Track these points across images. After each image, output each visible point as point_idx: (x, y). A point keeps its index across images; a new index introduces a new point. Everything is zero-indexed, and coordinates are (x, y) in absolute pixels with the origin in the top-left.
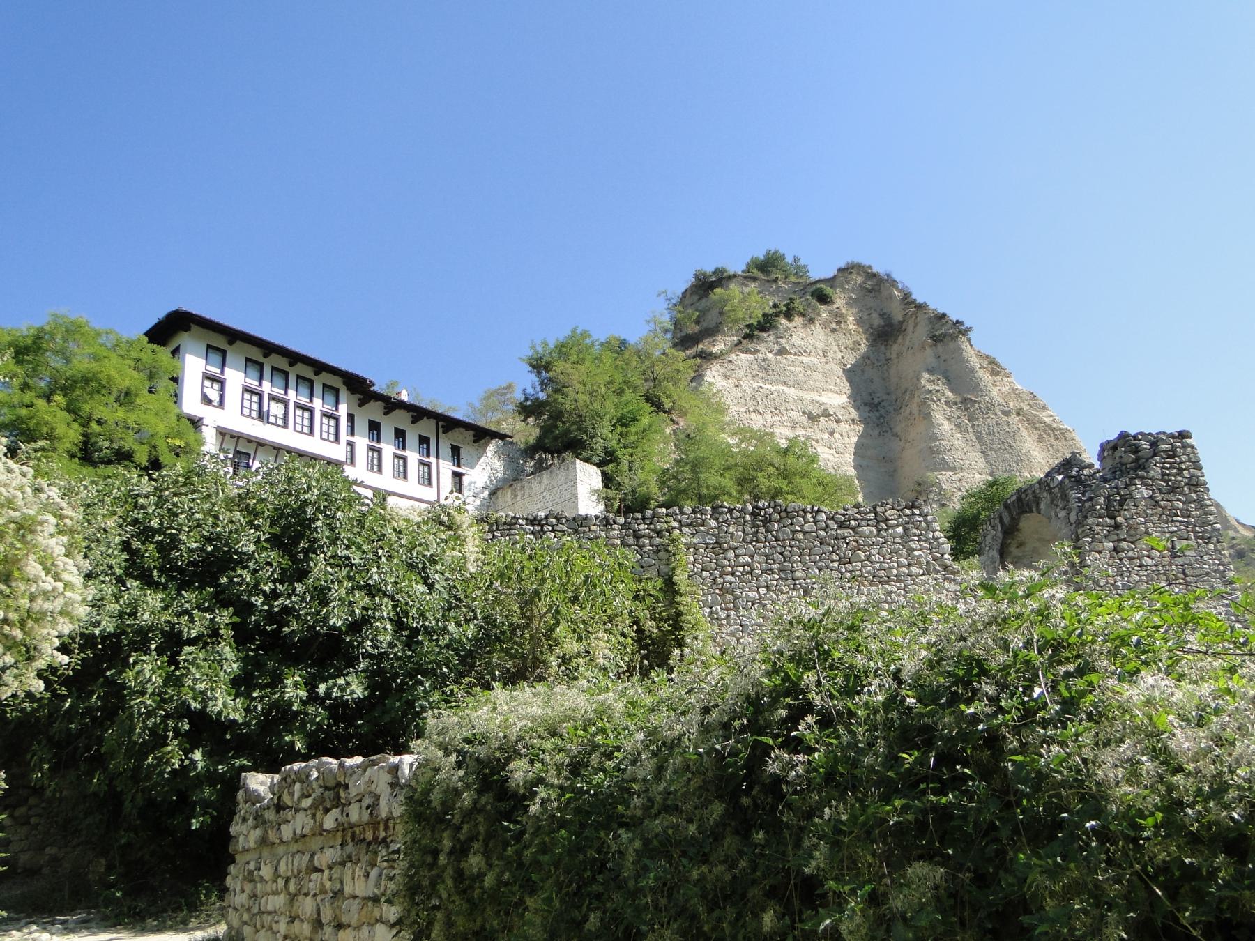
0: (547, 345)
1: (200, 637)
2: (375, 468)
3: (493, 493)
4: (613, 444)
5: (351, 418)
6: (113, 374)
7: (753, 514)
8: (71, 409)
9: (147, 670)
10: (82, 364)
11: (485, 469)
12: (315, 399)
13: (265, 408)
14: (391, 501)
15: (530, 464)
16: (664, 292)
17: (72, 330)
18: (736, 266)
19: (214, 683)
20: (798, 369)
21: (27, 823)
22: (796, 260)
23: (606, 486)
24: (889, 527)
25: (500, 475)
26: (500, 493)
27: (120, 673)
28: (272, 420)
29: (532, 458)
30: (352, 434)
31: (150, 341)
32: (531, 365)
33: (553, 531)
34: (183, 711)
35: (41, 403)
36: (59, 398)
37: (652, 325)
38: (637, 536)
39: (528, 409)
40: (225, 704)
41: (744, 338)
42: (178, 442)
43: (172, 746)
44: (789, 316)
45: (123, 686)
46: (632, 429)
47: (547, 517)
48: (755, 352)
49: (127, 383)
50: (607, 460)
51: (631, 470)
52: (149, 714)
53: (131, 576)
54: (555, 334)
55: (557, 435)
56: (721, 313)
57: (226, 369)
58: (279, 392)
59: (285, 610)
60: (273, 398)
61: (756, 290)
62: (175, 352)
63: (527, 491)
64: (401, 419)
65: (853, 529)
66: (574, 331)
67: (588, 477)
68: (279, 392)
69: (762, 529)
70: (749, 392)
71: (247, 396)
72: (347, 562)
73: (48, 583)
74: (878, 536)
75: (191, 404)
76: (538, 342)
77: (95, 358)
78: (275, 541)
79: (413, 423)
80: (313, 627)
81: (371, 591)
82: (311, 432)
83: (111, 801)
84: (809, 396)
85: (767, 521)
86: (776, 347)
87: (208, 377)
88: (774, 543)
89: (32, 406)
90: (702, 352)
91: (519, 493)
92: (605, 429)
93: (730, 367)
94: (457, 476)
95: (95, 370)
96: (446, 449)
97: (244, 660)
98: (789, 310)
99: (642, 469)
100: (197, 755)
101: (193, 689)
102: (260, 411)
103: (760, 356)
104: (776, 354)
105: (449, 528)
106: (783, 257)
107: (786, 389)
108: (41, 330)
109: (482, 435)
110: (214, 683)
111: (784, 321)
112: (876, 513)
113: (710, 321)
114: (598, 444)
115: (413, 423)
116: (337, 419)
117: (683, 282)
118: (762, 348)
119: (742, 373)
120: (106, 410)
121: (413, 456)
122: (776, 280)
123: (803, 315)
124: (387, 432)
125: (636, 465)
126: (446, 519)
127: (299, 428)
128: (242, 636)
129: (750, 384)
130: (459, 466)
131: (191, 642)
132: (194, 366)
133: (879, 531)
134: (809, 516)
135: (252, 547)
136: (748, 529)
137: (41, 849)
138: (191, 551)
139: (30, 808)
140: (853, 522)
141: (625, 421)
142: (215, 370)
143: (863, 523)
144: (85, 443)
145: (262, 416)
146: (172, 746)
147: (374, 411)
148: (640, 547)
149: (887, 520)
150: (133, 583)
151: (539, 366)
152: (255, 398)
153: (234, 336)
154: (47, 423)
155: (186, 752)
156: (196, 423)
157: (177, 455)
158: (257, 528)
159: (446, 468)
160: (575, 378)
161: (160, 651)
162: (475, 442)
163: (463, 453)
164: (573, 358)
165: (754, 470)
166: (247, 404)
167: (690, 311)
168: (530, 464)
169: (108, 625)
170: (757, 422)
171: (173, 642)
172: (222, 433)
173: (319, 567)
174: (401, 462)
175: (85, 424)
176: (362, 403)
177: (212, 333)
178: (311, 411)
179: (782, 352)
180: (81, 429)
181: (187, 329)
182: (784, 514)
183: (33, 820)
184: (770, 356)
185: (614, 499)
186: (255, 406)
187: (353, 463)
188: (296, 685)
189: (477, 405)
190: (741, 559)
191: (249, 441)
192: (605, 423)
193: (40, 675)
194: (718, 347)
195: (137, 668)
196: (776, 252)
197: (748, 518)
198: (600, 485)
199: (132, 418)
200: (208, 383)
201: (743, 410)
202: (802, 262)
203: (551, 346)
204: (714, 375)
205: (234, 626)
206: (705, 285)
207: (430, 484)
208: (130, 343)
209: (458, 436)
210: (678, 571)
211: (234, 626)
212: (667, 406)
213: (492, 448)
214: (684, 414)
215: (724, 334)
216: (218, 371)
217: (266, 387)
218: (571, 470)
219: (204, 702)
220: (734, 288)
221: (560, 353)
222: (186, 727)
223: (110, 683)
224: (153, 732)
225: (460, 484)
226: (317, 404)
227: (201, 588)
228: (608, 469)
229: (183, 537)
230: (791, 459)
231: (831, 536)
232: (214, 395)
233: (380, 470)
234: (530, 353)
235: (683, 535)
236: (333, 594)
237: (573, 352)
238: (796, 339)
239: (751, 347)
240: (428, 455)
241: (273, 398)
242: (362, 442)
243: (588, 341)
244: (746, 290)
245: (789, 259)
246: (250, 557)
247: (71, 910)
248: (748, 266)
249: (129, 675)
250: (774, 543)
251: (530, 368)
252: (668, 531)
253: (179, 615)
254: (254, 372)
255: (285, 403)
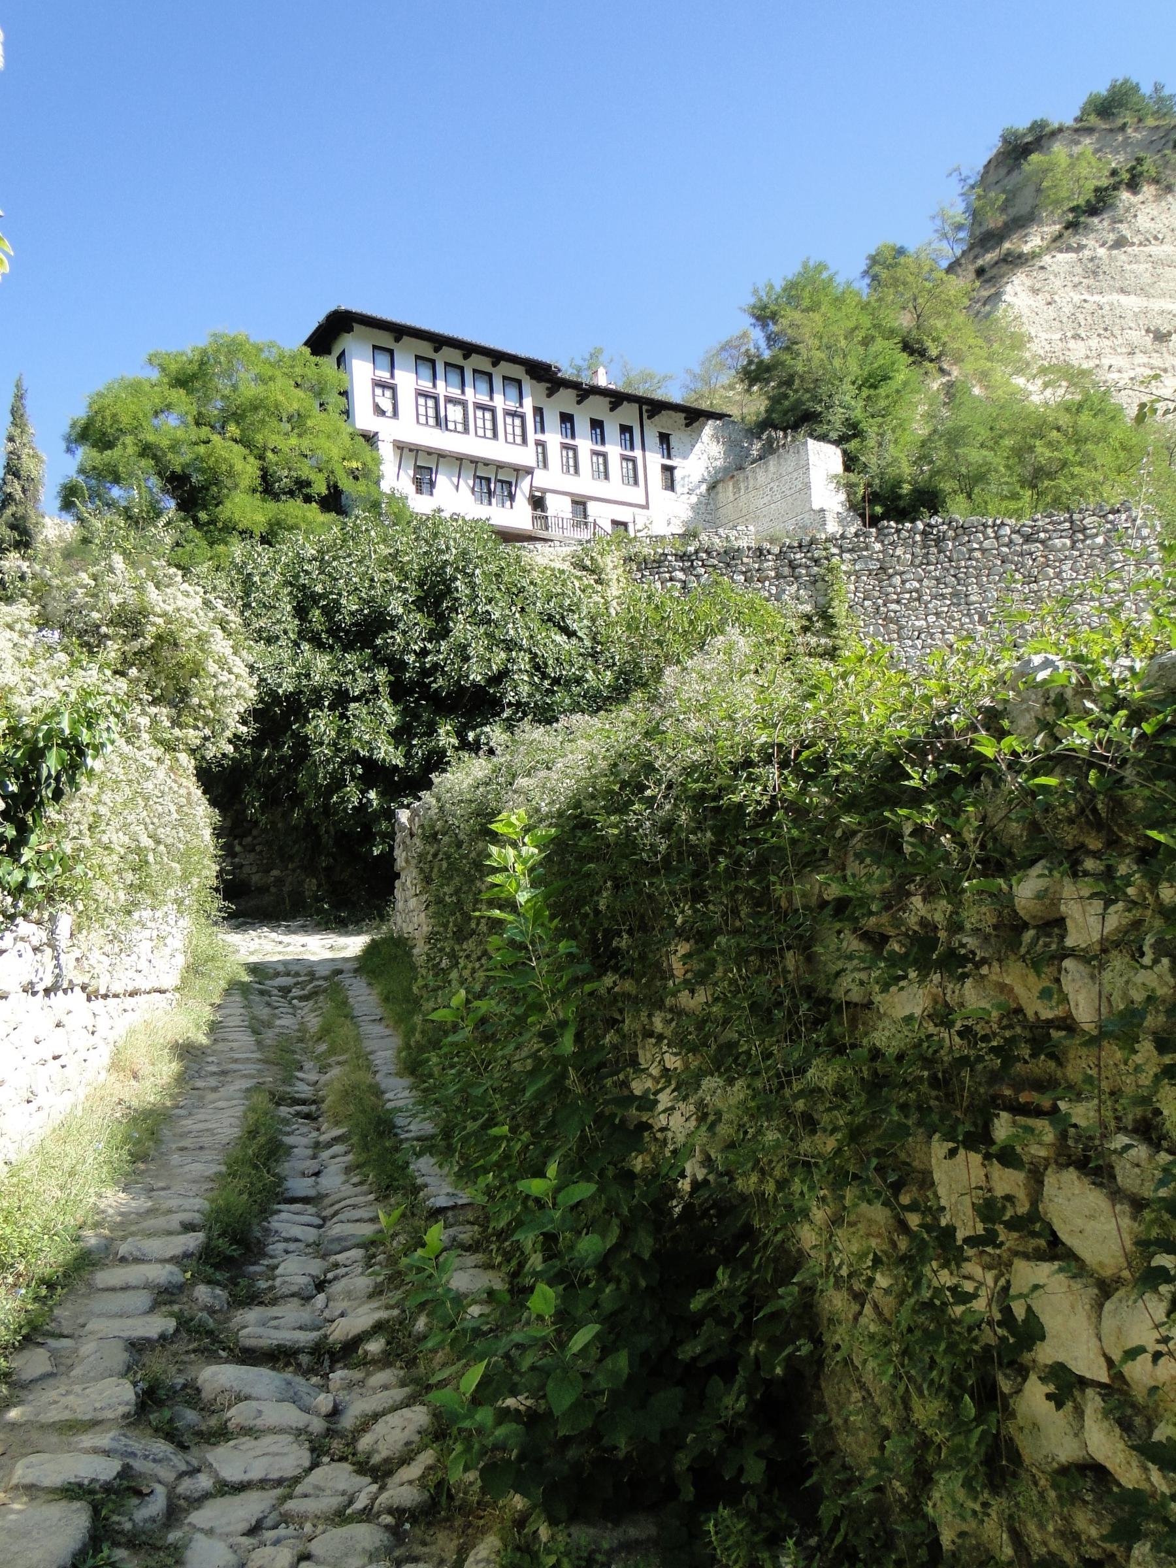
0: (772, 287)
1: (364, 693)
2: (572, 470)
3: (712, 487)
4: (858, 414)
5: (538, 411)
6: (281, 398)
7: (924, 533)
8: (245, 442)
9: (322, 725)
10: (250, 390)
11: (703, 454)
12: (496, 396)
13: (442, 414)
14: (591, 507)
15: (757, 446)
16: (957, 169)
17: (234, 348)
18: (1064, 114)
19: (376, 733)
20: (1142, 267)
21: (253, 850)
22: (1158, 88)
23: (847, 468)
24: (1086, 537)
25: (718, 463)
26: (720, 487)
27: (303, 726)
28: (451, 426)
29: (759, 438)
30: (543, 431)
31: (314, 353)
32: (753, 315)
33: (703, 566)
34: (355, 758)
35: (216, 438)
36: (233, 429)
37: (938, 222)
38: (793, 566)
39: (755, 373)
40: (388, 752)
41: (1067, 228)
42: (354, 465)
43: (351, 787)
44: (1133, 185)
45: (306, 738)
46: (882, 391)
47: (697, 552)
48: (1081, 247)
49: (296, 406)
50: (851, 433)
51: (880, 445)
52: (328, 761)
53: (303, 638)
54: (777, 272)
55: (789, 411)
56: (1039, 190)
57: (396, 372)
58: (455, 392)
59: (435, 666)
60: (449, 400)
61: (1090, 149)
62: (341, 360)
63: (751, 482)
64: (598, 407)
65: (1042, 542)
66: (805, 265)
67: (823, 460)
68: (455, 392)
69: (934, 550)
70: (1068, 309)
71: (421, 401)
72: (486, 620)
73: (224, 677)
74: (1073, 548)
75: (364, 419)
76: (761, 285)
77: (261, 379)
78: (420, 604)
79: (612, 410)
80: (458, 681)
81: (510, 645)
82: (495, 435)
83: (310, 830)
84: (1157, 304)
85: (940, 540)
86: (1112, 237)
87: (379, 384)
88: (946, 565)
89: (208, 442)
90: (1009, 253)
91: (742, 486)
92: (847, 393)
93: (1042, 275)
94: (668, 470)
95: (262, 396)
96: (652, 439)
97: (405, 712)
98: (1133, 177)
99: (896, 442)
100: (372, 795)
101: (359, 739)
102: (437, 417)
103: (1087, 253)
104: (1112, 247)
105: (593, 572)
106: (1136, 88)
107: (1123, 299)
108: (204, 352)
109: (694, 416)
110: (376, 733)
111: (1125, 195)
112: (1072, 522)
113: (1021, 207)
114: (837, 416)
115: (612, 410)
116: (522, 417)
117: (987, 146)
118: (1090, 241)
119: (1058, 283)
120: (279, 439)
121: (614, 450)
122: (1123, 128)
123: (1156, 181)
124: (582, 425)
125: (889, 436)
126: (588, 563)
127: (480, 432)
128: (398, 692)
129: (1068, 298)
130: (669, 457)
131: (356, 699)
132: (362, 371)
133: (1074, 542)
134: (989, 530)
135: (401, 610)
136: (917, 550)
137: (267, 872)
138: (352, 614)
139: (255, 838)
140: (1042, 535)
141: (874, 381)
142: (384, 375)
143: (1055, 535)
144: (264, 477)
145: (440, 422)
146: (351, 787)
147: (565, 400)
148: (796, 578)
149: (1085, 529)
150: (305, 646)
151: (764, 316)
152: (431, 403)
153: (400, 332)
154: (225, 460)
155: (363, 792)
156: (370, 439)
157: (356, 478)
158: (404, 591)
159: (654, 460)
160: (806, 332)
161: (332, 707)
162: (687, 425)
163: (673, 441)
164: (806, 303)
165: (1034, 436)
166: (422, 410)
167: (992, 194)
168: (757, 446)
169: (288, 686)
170: (1077, 354)
171: (342, 698)
172: (401, 447)
173: (460, 627)
174: (601, 460)
175: (261, 457)
176: (550, 393)
177: (376, 331)
178: (493, 411)
179: (1120, 243)
180: (258, 463)
181: (349, 330)
182: (960, 531)
183: (258, 848)
184: (1102, 252)
185: (856, 485)
186: (431, 412)
187: (545, 466)
188: (448, 733)
189: (697, 370)
190: (908, 585)
191: (429, 454)
192: (847, 386)
193: (230, 741)
194: (1033, 241)
195: (314, 723)
196: (1126, 81)
197: (918, 538)
198: (839, 468)
199: (305, 443)
200: (378, 391)
201: (1058, 336)
202: (1166, 92)
203: (778, 289)
204: (1017, 294)
205: (391, 684)
206: (1017, 150)
207: (636, 483)
208: (293, 358)
209: (665, 421)
210: (835, 603)
211: (391, 684)
212: (933, 352)
213: (709, 429)
214: (958, 360)
215: (1041, 223)
216: (388, 375)
217: (441, 389)
218: (801, 451)
219: (371, 750)
220: (1059, 150)
221: (790, 297)
222: (360, 771)
223: (295, 735)
224: (333, 775)
225: (672, 481)
226: (499, 401)
227: (362, 649)
228: (853, 445)
229: (343, 601)
230: (1085, 417)
231: (1015, 553)
232: (386, 405)
233: (577, 471)
234: (752, 300)
235: (843, 561)
236: (471, 652)
237: (806, 294)
238: (1143, 222)
239: (1073, 241)
240: (632, 448)
241: (449, 400)
242: (554, 438)
243: (825, 275)
244: (1076, 150)
245: (1146, 89)
246: (400, 618)
247: (294, 918)
248: (1085, 111)
249: (309, 729)
250: (946, 565)
251: (753, 321)
252: (827, 558)
253: (345, 674)
254: (426, 371)
255: (464, 404)
